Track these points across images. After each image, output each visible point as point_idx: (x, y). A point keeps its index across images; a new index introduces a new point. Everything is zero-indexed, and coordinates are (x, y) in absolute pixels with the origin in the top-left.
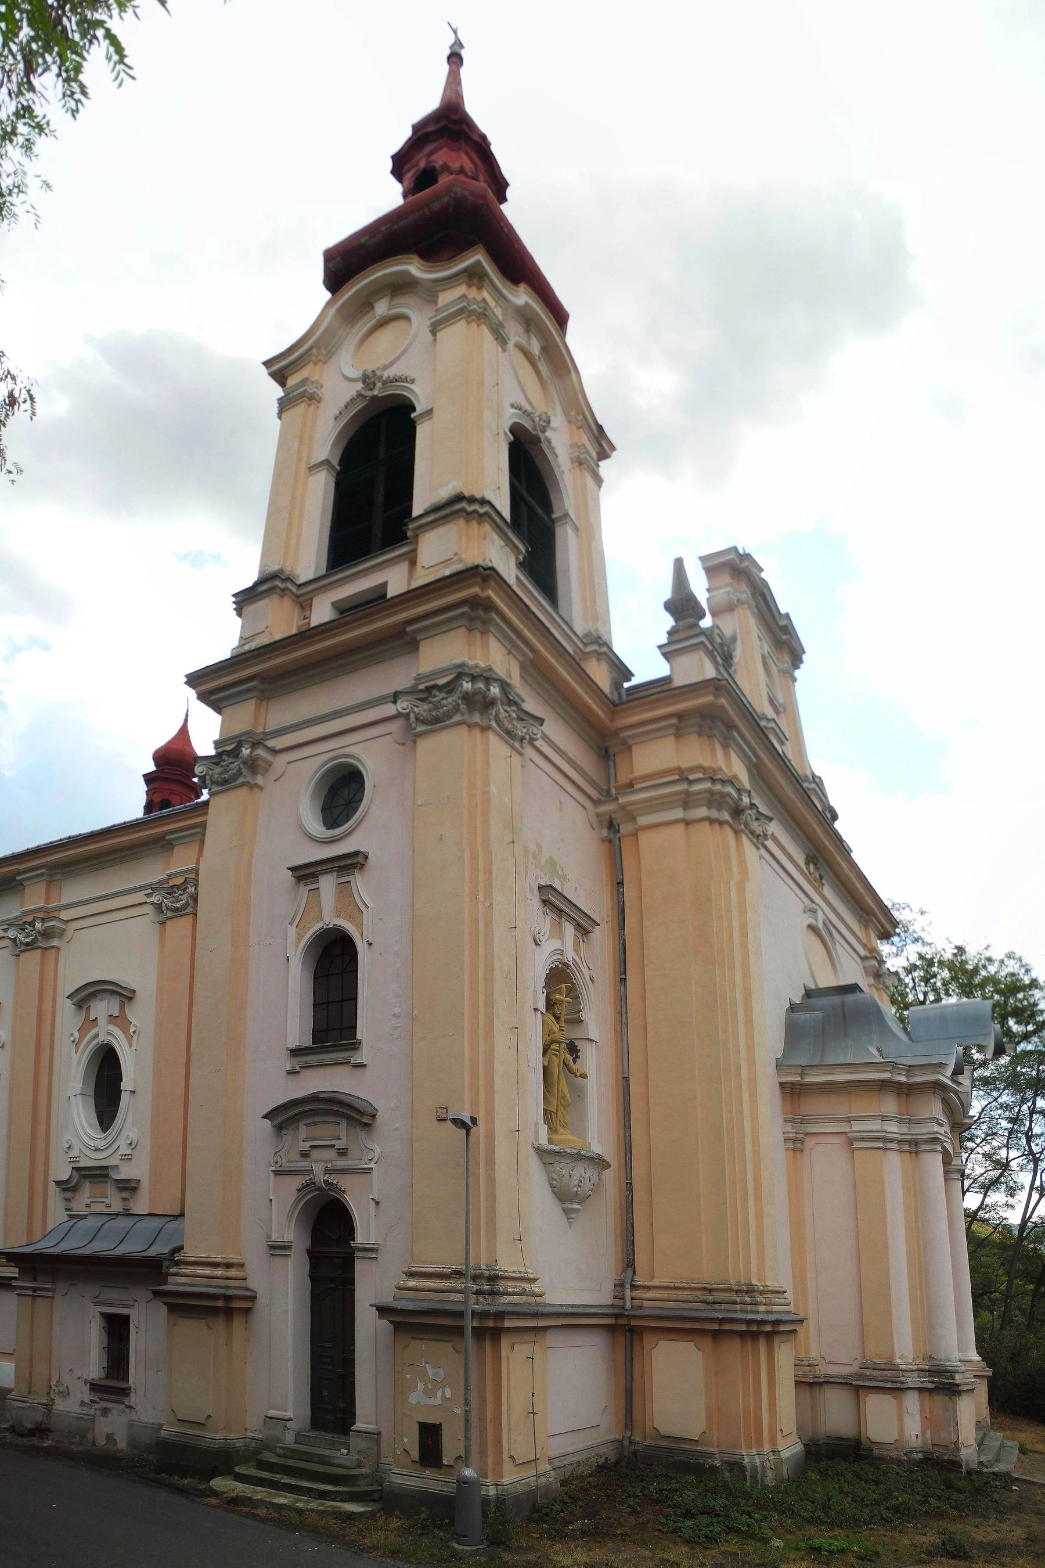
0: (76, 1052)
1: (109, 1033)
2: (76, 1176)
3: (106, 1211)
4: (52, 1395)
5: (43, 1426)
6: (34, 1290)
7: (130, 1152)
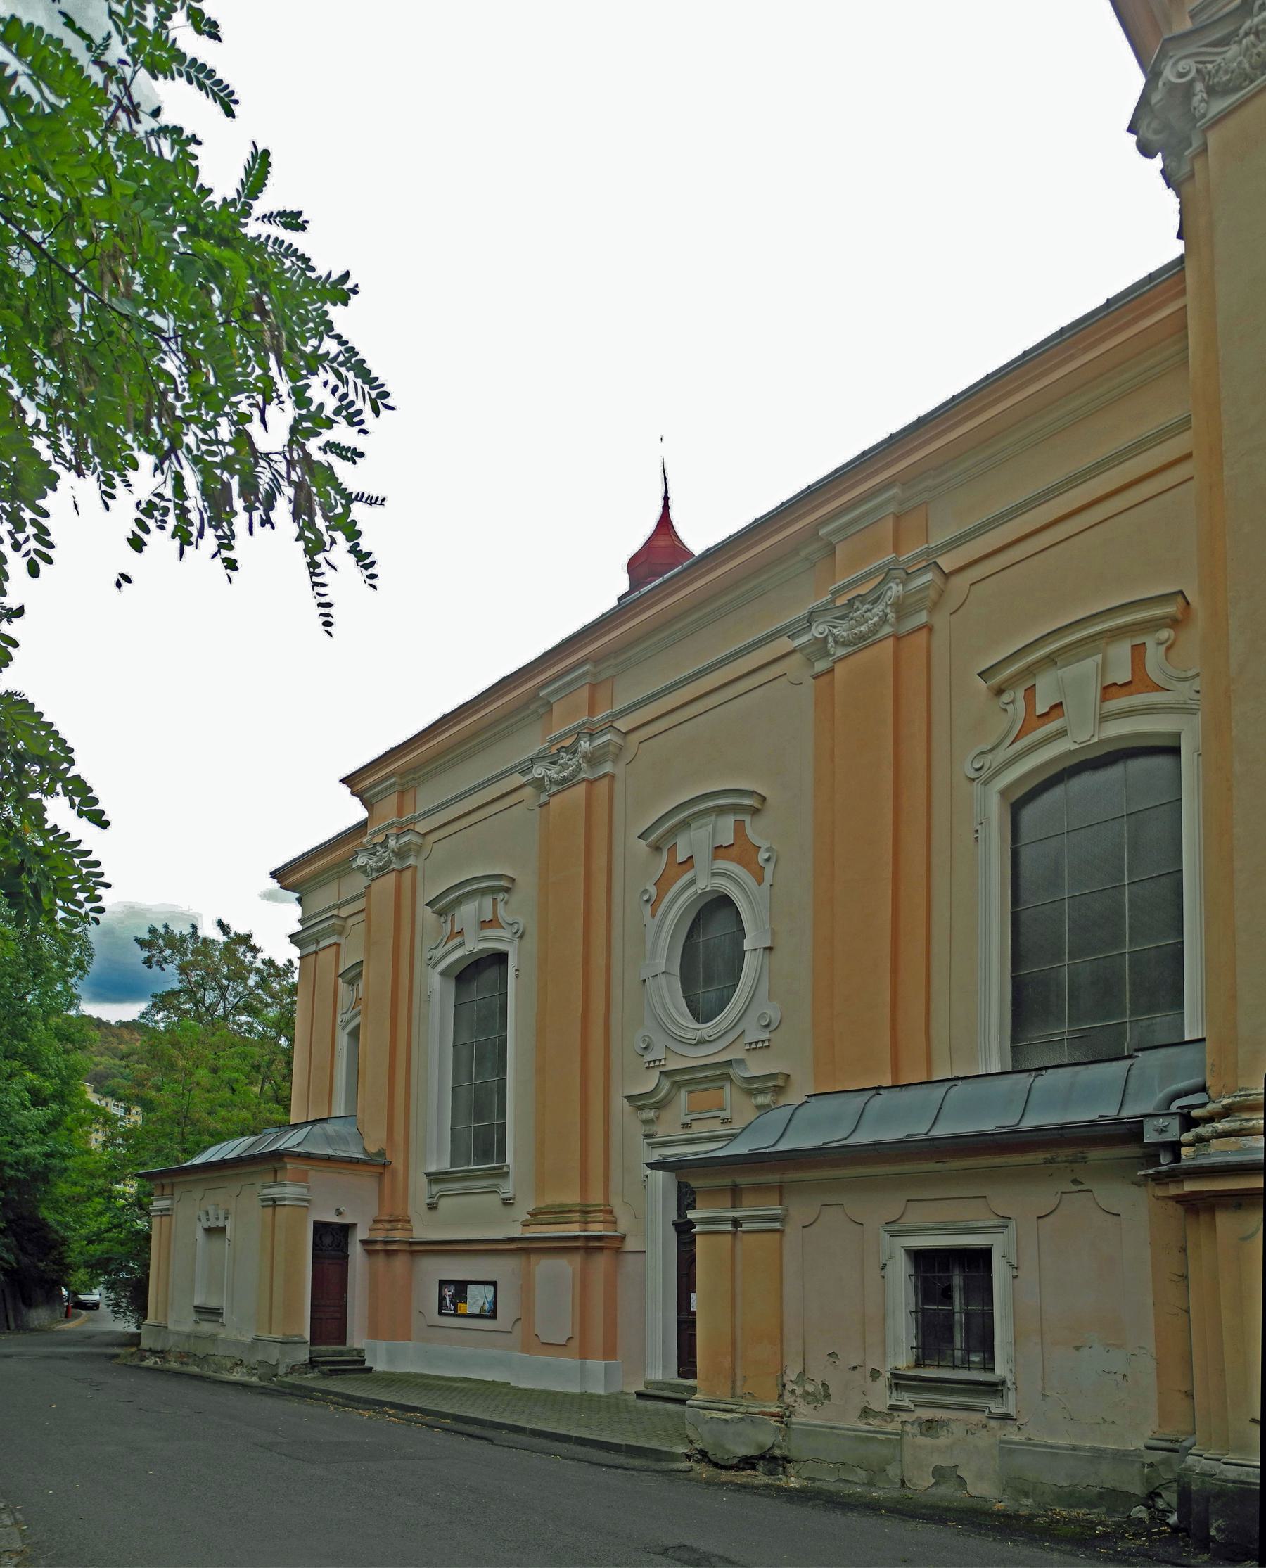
0: (653, 916)
1: (714, 874)
2: (666, 1085)
3: (725, 1130)
4: (788, 1399)
5: (777, 1452)
6: (736, 1222)
7: (766, 1036)
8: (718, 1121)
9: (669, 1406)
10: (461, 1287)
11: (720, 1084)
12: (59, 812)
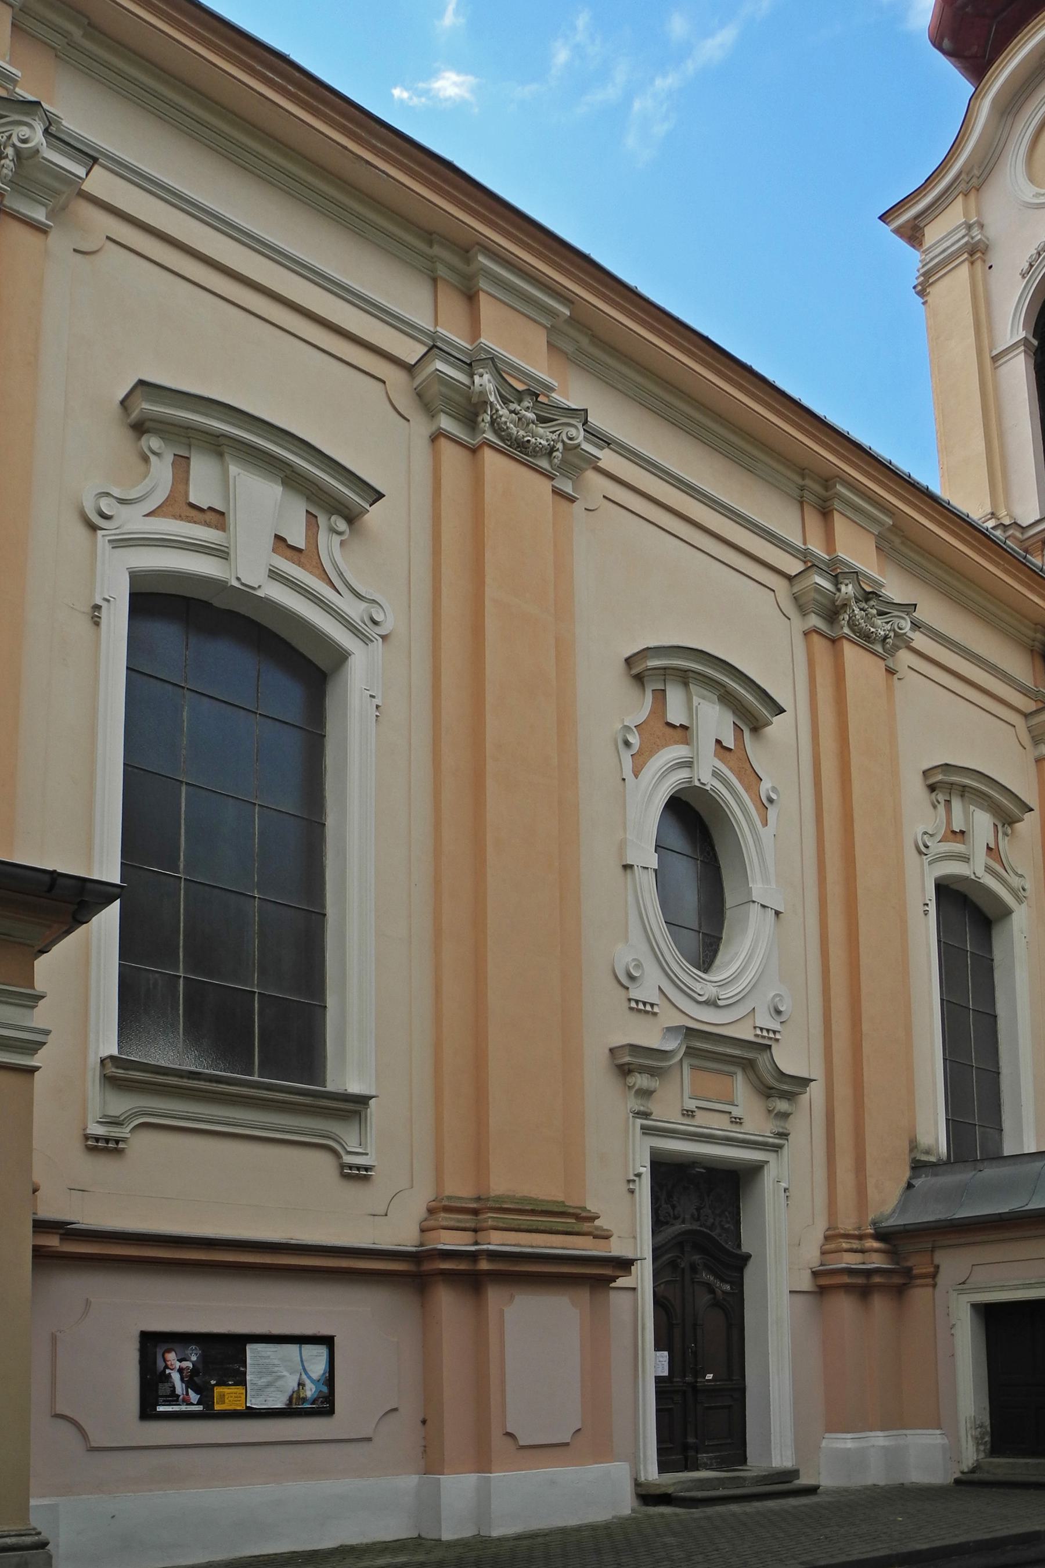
8: (726, 1117)
9: (735, 1508)
10: (222, 1356)
11: (732, 1069)
12: (1035, 343)
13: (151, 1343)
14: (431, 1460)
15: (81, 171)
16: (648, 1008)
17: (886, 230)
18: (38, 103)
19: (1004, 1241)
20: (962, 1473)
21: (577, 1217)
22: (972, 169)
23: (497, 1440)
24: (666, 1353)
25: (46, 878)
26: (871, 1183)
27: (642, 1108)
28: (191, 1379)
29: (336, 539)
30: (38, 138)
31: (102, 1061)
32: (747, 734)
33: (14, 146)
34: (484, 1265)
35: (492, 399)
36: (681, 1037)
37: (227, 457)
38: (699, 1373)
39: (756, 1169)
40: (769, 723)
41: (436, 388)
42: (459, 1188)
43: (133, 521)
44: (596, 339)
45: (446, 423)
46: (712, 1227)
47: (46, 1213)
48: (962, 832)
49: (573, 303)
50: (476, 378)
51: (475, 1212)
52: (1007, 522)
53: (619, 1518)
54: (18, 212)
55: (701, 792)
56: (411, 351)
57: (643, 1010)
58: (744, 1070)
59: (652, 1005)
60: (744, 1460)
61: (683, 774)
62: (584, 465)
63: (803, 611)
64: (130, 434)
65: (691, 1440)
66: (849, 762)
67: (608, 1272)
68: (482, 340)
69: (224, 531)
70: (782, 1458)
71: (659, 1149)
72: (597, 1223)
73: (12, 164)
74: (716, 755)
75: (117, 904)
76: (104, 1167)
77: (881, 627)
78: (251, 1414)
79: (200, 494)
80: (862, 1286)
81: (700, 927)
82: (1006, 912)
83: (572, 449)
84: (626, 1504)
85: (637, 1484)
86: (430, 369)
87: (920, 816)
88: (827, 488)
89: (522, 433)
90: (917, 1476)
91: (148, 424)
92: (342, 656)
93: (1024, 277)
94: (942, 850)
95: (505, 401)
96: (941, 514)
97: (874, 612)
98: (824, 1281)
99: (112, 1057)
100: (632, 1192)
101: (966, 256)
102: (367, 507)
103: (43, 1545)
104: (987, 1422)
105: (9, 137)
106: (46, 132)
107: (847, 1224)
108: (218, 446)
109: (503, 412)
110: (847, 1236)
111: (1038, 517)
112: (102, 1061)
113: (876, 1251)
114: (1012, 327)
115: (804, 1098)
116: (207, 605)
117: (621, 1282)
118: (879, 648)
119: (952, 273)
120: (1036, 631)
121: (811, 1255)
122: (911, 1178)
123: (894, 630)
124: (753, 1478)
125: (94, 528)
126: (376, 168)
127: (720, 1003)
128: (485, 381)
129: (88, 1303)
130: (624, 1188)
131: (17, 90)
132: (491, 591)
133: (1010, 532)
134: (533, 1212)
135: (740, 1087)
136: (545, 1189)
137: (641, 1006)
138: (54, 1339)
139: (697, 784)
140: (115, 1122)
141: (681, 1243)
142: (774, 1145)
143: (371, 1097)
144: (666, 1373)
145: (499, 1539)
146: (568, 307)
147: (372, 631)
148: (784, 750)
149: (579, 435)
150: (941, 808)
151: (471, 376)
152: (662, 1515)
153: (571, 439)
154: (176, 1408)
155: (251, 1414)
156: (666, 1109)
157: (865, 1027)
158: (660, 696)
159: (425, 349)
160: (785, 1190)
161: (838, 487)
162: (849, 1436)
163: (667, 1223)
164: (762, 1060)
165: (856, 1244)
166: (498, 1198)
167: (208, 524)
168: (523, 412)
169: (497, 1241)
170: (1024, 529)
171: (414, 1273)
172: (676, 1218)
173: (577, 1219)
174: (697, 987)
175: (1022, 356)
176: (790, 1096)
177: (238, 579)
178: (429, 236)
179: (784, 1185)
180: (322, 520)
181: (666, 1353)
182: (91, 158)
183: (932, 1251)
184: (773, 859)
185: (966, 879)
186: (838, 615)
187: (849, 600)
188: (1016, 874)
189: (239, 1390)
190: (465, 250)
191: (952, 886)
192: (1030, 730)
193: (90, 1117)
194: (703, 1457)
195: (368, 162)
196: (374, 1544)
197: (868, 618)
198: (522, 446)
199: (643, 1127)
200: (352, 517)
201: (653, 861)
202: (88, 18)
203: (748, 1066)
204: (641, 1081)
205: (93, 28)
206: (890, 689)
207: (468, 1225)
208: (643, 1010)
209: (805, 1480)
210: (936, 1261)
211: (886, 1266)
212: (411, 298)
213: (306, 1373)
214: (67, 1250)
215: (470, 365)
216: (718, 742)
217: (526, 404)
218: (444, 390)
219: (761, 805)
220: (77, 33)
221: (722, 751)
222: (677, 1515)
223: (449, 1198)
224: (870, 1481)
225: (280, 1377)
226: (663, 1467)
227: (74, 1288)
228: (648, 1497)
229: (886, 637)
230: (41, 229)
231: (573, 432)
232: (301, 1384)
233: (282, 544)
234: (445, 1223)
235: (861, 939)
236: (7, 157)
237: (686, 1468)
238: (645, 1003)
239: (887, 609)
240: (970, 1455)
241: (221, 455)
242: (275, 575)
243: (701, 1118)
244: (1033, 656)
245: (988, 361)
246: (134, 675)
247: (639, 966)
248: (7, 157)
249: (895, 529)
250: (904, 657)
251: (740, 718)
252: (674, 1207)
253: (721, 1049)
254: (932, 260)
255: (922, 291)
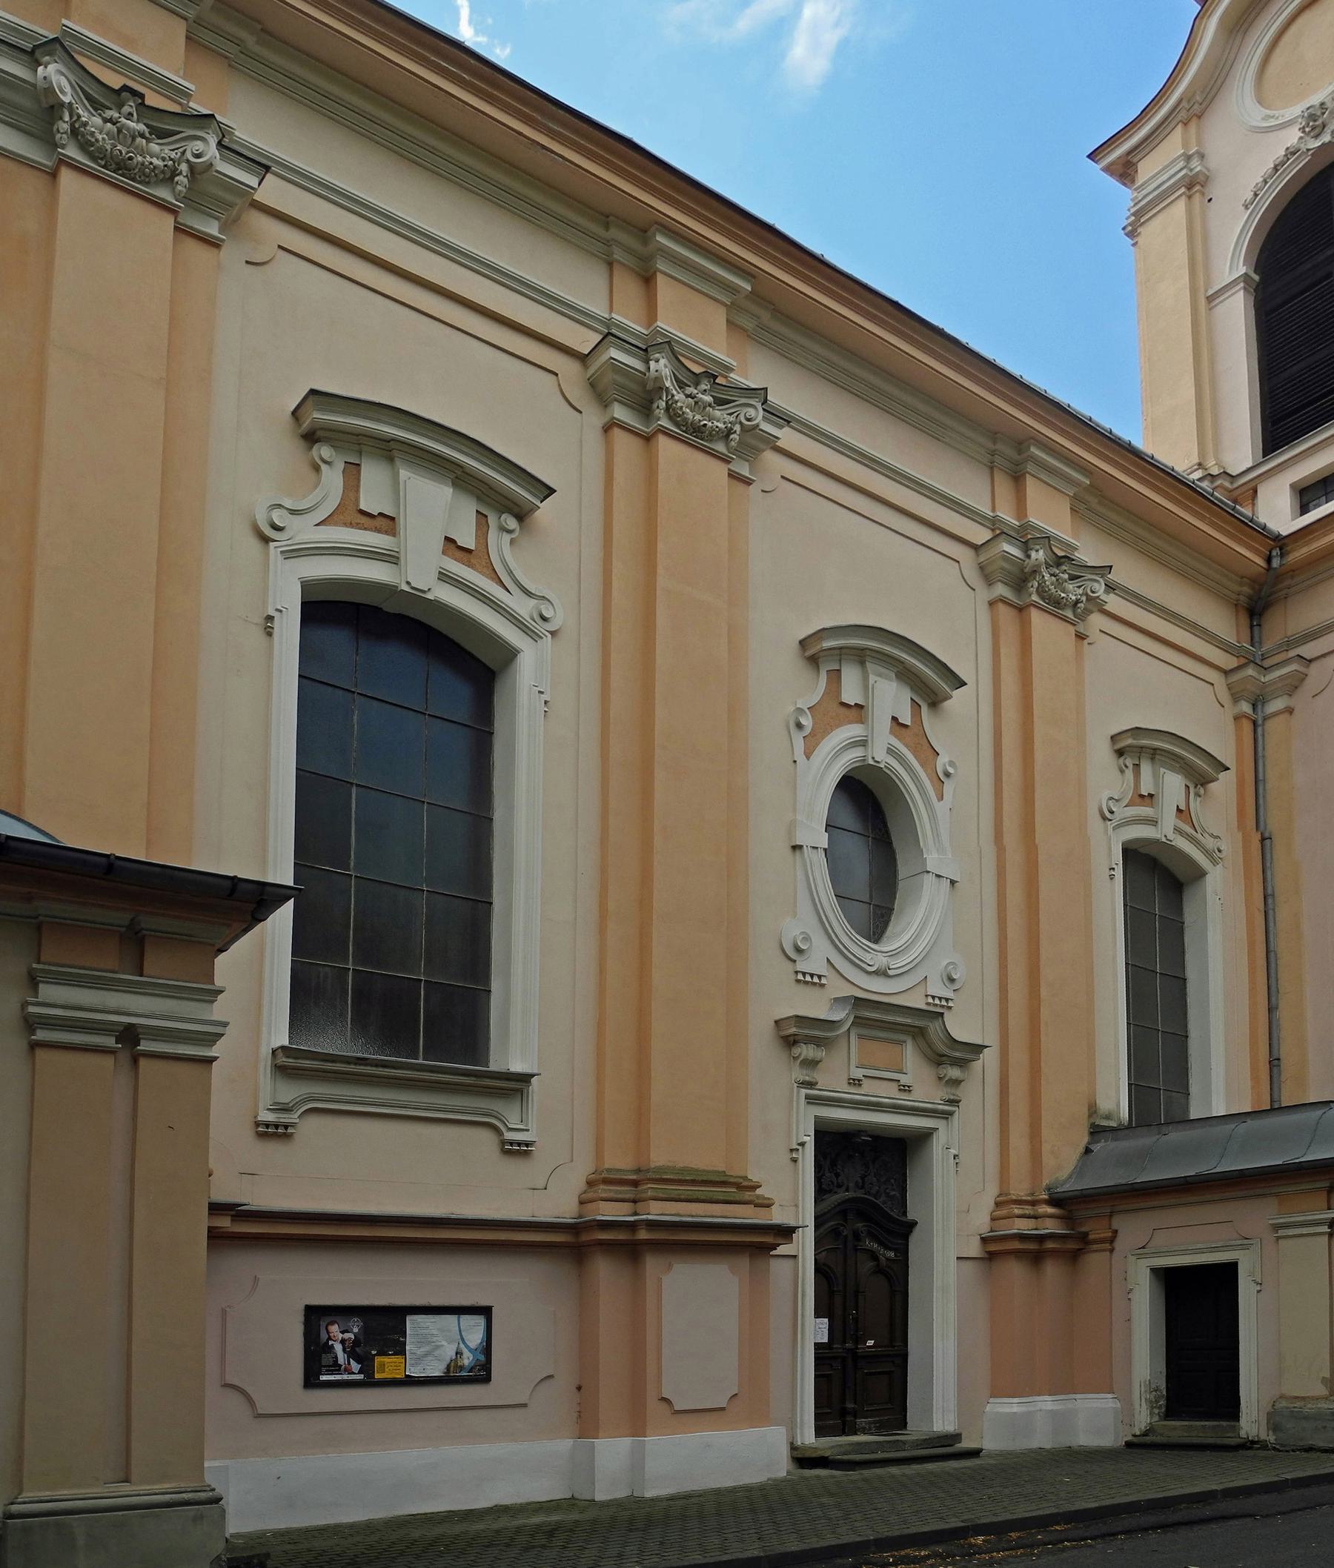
8: (895, 1085)
9: (894, 1470)
10: (384, 1327)
11: (902, 1037)
12: (1257, 278)
13: (315, 1315)
14: (586, 1424)
15: (253, 181)
16: (816, 980)
17: (1095, 168)
18: (212, 116)
19: (1171, 1206)
20: (1134, 1436)
21: (739, 1186)
22: (1194, 95)
23: (652, 1404)
24: (826, 1320)
25: (228, 883)
26: (1046, 1148)
27: (807, 1078)
28: (353, 1350)
29: (507, 538)
30: (212, 151)
31: (274, 1051)
32: (924, 708)
33: (188, 161)
34: (643, 1235)
35: (668, 384)
36: (849, 1007)
37: (398, 462)
38: (859, 1340)
39: (924, 1137)
40: (949, 697)
41: (610, 376)
42: (620, 1161)
43: (304, 531)
44: (777, 312)
45: (620, 412)
46: (877, 1195)
47: (222, 1194)
48: (1151, 796)
49: (754, 277)
50: (652, 363)
51: (635, 1183)
52: (1215, 471)
53: (775, 1480)
54: (191, 228)
55: (875, 770)
56: (584, 340)
57: (811, 981)
58: (914, 1038)
59: (820, 977)
60: (904, 1425)
61: (857, 753)
62: (762, 446)
63: (989, 580)
64: (301, 444)
65: (850, 1405)
66: (1032, 731)
67: (769, 1239)
68: (659, 323)
69: (394, 535)
70: (943, 1422)
71: (822, 1118)
72: (758, 1191)
73: (185, 180)
74: (891, 732)
75: (291, 902)
76: (273, 1148)
77: (1072, 591)
78: (410, 1382)
79: (371, 500)
80: (1034, 1251)
81: (871, 897)
82: (1200, 874)
83: (750, 430)
84: (782, 1467)
85: (793, 1448)
86: (604, 358)
87: (1105, 780)
88: (1020, 452)
89: (698, 417)
90: (1085, 1439)
91: (319, 433)
92: (510, 654)
93: (1247, 208)
94: (1128, 814)
95: (682, 385)
96: (1144, 470)
97: (1066, 576)
98: (993, 1248)
99: (283, 1048)
100: (795, 1161)
101: (1183, 190)
102: (538, 503)
103: (217, 1500)
104: (1163, 1386)
105: (183, 153)
106: (220, 144)
107: (1020, 1189)
108: (388, 450)
109: (679, 396)
110: (1019, 1202)
111: (1250, 465)
112: (274, 1051)
113: (1051, 1216)
114: (1231, 259)
115: (977, 1065)
116: (377, 610)
117: (782, 1250)
118: (1069, 614)
119: (1168, 210)
120: (1241, 584)
121: (981, 1221)
122: (1089, 1143)
123: (1087, 595)
124: (913, 1442)
125: (266, 540)
126: (552, 152)
127: (891, 973)
128: (661, 366)
129: (256, 1279)
130: (1108, 872)
131: (191, 104)
132: (662, 581)
133: (1218, 482)
134: (693, 1182)
135: (910, 1055)
136: (706, 1159)
137: (808, 978)
138: (224, 1312)
139: (871, 762)
140: (285, 1109)
141: (843, 1211)
142: (943, 1112)
143: (533, 1076)
144: (826, 1340)
145: (652, 1500)
146: (749, 281)
147: (540, 627)
148: (963, 726)
149: (757, 415)
150: (1129, 773)
151: (647, 361)
152: (818, 1477)
153: (749, 420)
154: (338, 1377)
155: (410, 1382)
156: (832, 1079)
157: (1044, 993)
158: (835, 676)
159: (600, 337)
160: (955, 1157)
161: (1033, 449)
162: (1016, 1400)
163: (830, 1191)
164: (933, 1028)
165: (1028, 1210)
166: (659, 1170)
167: (378, 530)
168: (700, 395)
169: (657, 1211)
170: (1233, 478)
171: (570, 1244)
172: (839, 1186)
173: (738, 1188)
174: (867, 958)
175: (1242, 292)
176: (962, 1063)
177: (408, 583)
178: (606, 219)
179: (953, 1151)
180: (492, 519)
181: (826, 1320)
182: (263, 167)
183: (1111, 1216)
184: (949, 833)
185: (1157, 842)
186: (1028, 583)
187: (1039, 566)
188: (1212, 835)
189: (399, 1359)
190: (643, 229)
191: (1142, 850)
192: (1229, 687)
193: (261, 1105)
194: (861, 1422)
195: (544, 147)
196: (529, 1504)
197: (1059, 584)
198: (698, 430)
199: (807, 1097)
200: (522, 515)
201: (823, 840)
202: (259, 22)
203: (919, 1033)
204: (807, 1051)
205: (267, 35)
206: (1079, 656)
207: (627, 1196)
208: (811, 981)
209: (966, 1444)
210: (1115, 1225)
211: (1060, 1232)
212: (582, 283)
213: (464, 1343)
214: (242, 1230)
215: (646, 350)
216: (894, 719)
217: (703, 387)
218: (618, 378)
219: (935, 779)
220: (250, 41)
221: (897, 728)
222: (834, 1477)
223: (609, 1170)
224: (1035, 1444)
225: (438, 1347)
226: (820, 1431)
227: (245, 1265)
228: (803, 1460)
229: (1077, 602)
230: (214, 243)
231: (751, 412)
232: (459, 1353)
233: (452, 546)
234: (604, 1195)
235: (1042, 906)
236: (181, 173)
237: (844, 1433)
238: (812, 975)
239: (1080, 572)
240: (1143, 1418)
241: (391, 460)
242: (444, 577)
243: (868, 1087)
244: (1237, 612)
245: (1203, 301)
246: (305, 681)
247: (807, 938)
248: (181, 173)
249: (1093, 489)
250: (1097, 620)
251: (916, 692)
252: (837, 1175)
253: (890, 1018)
254: (1145, 197)
255: (1132, 232)
